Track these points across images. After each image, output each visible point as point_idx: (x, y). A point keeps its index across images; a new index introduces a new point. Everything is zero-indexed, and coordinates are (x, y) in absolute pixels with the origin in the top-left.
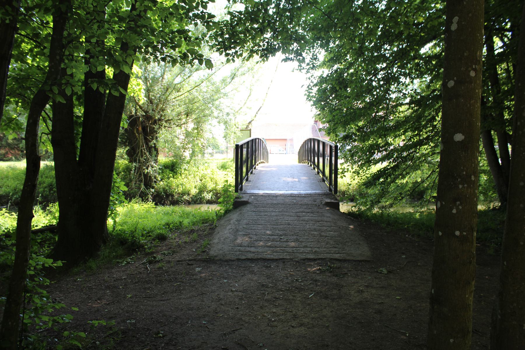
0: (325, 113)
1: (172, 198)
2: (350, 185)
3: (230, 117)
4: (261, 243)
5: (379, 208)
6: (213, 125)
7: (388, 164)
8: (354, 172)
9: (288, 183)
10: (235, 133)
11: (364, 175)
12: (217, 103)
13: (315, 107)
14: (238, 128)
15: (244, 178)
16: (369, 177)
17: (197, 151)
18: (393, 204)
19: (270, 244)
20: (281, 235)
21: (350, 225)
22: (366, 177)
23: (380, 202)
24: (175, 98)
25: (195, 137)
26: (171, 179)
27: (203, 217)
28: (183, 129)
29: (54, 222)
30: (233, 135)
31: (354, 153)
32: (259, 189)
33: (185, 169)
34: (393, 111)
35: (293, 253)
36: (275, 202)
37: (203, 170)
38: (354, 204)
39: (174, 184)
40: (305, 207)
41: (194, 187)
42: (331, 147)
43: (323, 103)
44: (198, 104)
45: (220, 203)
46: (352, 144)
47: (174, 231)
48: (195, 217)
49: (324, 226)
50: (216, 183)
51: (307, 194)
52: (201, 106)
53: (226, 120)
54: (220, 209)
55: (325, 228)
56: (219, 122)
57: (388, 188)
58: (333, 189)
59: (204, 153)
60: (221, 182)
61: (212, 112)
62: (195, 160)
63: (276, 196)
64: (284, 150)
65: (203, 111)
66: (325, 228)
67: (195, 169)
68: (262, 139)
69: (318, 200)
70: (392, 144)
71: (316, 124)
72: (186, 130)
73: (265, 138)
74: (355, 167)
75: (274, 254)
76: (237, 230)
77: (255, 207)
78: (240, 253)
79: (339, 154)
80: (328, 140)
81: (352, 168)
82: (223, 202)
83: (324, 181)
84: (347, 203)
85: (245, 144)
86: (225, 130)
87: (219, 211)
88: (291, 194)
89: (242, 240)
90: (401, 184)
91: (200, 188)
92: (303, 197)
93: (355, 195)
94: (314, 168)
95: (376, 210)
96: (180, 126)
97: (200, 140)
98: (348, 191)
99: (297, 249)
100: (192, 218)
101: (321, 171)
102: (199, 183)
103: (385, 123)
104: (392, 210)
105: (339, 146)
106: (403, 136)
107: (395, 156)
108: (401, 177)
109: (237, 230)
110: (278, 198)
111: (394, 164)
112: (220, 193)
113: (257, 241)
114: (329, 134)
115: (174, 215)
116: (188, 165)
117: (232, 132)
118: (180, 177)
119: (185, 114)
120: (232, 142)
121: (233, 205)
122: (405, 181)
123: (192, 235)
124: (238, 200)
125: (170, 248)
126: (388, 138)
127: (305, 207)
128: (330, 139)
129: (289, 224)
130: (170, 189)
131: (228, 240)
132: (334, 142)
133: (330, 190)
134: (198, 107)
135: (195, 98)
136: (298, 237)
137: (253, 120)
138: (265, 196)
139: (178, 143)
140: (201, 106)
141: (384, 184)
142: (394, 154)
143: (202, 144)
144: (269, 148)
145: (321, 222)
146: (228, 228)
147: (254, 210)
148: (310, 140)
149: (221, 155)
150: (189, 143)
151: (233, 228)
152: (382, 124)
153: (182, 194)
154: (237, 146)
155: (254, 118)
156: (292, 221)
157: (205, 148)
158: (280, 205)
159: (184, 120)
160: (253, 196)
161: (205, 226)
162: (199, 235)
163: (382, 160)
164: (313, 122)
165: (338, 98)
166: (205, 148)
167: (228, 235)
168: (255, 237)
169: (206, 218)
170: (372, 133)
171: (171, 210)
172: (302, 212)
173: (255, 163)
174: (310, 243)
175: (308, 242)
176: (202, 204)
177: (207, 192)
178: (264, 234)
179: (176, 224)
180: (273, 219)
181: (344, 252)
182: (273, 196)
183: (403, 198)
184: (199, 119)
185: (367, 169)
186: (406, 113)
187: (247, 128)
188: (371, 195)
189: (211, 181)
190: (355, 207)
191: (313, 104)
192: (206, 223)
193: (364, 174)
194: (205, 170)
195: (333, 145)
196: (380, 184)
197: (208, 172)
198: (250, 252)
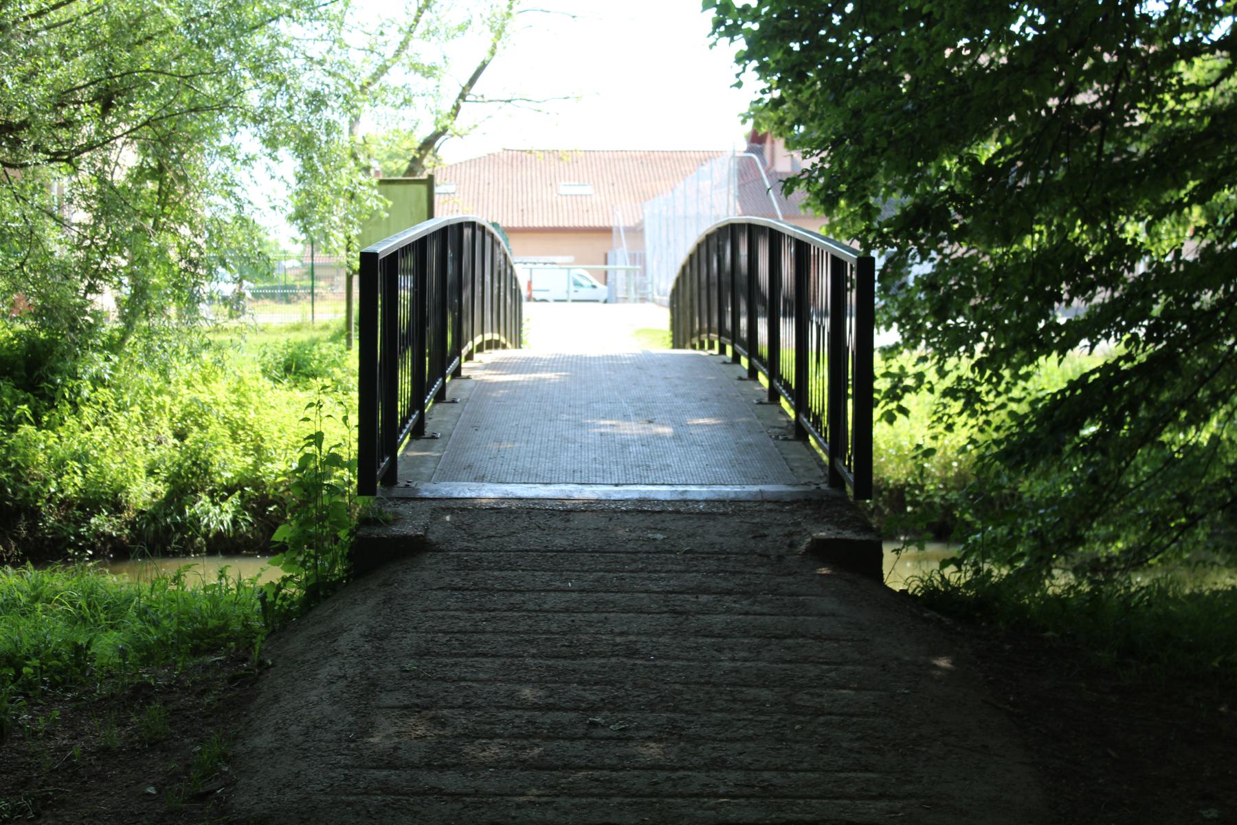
0: (806, 94)
1: (32, 528)
2: (930, 453)
3: (326, 114)
4: (494, 750)
5: (1075, 571)
6: (241, 157)
7: (1122, 350)
8: (950, 393)
9: (624, 445)
10: (353, 196)
11: (1003, 406)
12: (259, 40)
13: (755, 63)
14: (367, 169)
15: (404, 421)
16: (1026, 416)
17: (157, 288)
18: (1147, 548)
19: (537, 751)
20: (593, 709)
21: (938, 654)
22: (1012, 414)
23: (1081, 541)
24: (40, 13)
25: (146, 215)
26: (27, 429)
27: (193, 619)
28: (84, 176)
29: (1229, 61)
30: (341, 208)
31: (949, 294)
32: (481, 479)
33: (98, 381)
34: (1149, 85)
35: (657, 795)
36: (559, 542)
37: (189, 384)
38: (955, 551)
39: (41, 457)
40: (713, 564)
41: (143, 471)
42: (838, 265)
43: (796, 47)
44: (160, 49)
45: (282, 548)
46: (940, 252)
47: (44, 693)
48: (156, 624)
49: (806, 660)
50: (258, 449)
51: (722, 502)
52: (178, 58)
53: (306, 130)
54: (285, 580)
55: (813, 671)
56: (272, 142)
57: (1121, 472)
58: (851, 477)
59: (194, 300)
60: (282, 443)
61: (238, 92)
62: (150, 333)
63: (565, 512)
64: (601, 286)
65: (188, 80)
66: (813, 671)
67: (148, 377)
68: (489, 227)
69: (775, 532)
70: (1136, 252)
71: (760, 152)
72: (102, 181)
73: (504, 223)
74: (961, 366)
75: (560, 800)
76: (374, 686)
77: (463, 566)
78: (389, 798)
79: (879, 303)
80: (823, 232)
81: (942, 374)
82: (297, 544)
83: (800, 433)
84: (921, 548)
85: (405, 250)
86: (301, 179)
87: (279, 588)
88: (642, 501)
89: (399, 734)
90: (1186, 448)
91: (178, 475)
92: (701, 513)
93: (954, 505)
94: (753, 374)
95: (1060, 581)
96: (67, 157)
97: (175, 233)
98: (921, 488)
99: (675, 775)
100: (138, 625)
101: (787, 386)
102: (169, 451)
103: (1108, 147)
104: (1140, 579)
105: (880, 263)
106: (1197, 210)
107: (1157, 310)
108: (1183, 414)
109: (374, 686)
110: (577, 520)
111: (1150, 348)
112: (279, 501)
113: (471, 736)
114: (828, 202)
115: (45, 611)
116: (116, 359)
117: (338, 193)
118: (70, 421)
119: (97, 98)
120: (338, 239)
121: (350, 557)
122: (1204, 437)
123: (138, 713)
124: (377, 532)
125: (25, 783)
126: (1123, 219)
127: (713, 564)
128: (831, 227)
129: (631, 652)
130: (18, 479)
131: (329, 736)
132: (856, 245)
133: (835, 478)
134: (160, 67)
135: (143, 16)
136: (676, 716)
137: (445, 130)
138: (510, 511)
139: (57, 244)
140: (178, 58)
141: (1104, 452)
142: (1156, 301)
143: (183, 255)
144: (522, 274)
145: (790, 641)
146: (324, 673)
147: (458, 581)
148: (730, 232)
149: (283, 307)
150: (116, 244)
151: (350, 672)
152: (1091, 149)
153: (80, 507)
154: (368, 259)
155: (447, 122)
156: (646, 634)
157: (201, 271)
158: (584, 557)
159: (88, 130)
160: (448, 510)
161: (206, 668)
162: (174, 712)
163: (1091, 328)
164: (744, 145)
165: (870, 16)
166: (201, 271)
167: (328, 709)
168: (462, 720)
169: (212, 623)
170: (1042, 195)
171: (26, 587)
172: (699, 590)
173: (459, 343)
174: (738, 746)
175: (728, 740)
176: (187, 554)
177: (211, 494)
178: (506, 702)
179: (57, 656)
180: (554, 627)
181: (909, 788)
182: (552, 513)
183: (1193, 520)
184: (167, 126)
185: (1016, 376)
186: (1210, 94)
187: (411, 171)
188: (1036, 506)
189: (234, 437)
190: (958, 563)
191: (745, 48)
192: (212, 650)
193: (1003, 399)
194: (200, 387)
195: (850, 258)
196: (1084, 450)
197: (220, 390)
198: (440, 792)
